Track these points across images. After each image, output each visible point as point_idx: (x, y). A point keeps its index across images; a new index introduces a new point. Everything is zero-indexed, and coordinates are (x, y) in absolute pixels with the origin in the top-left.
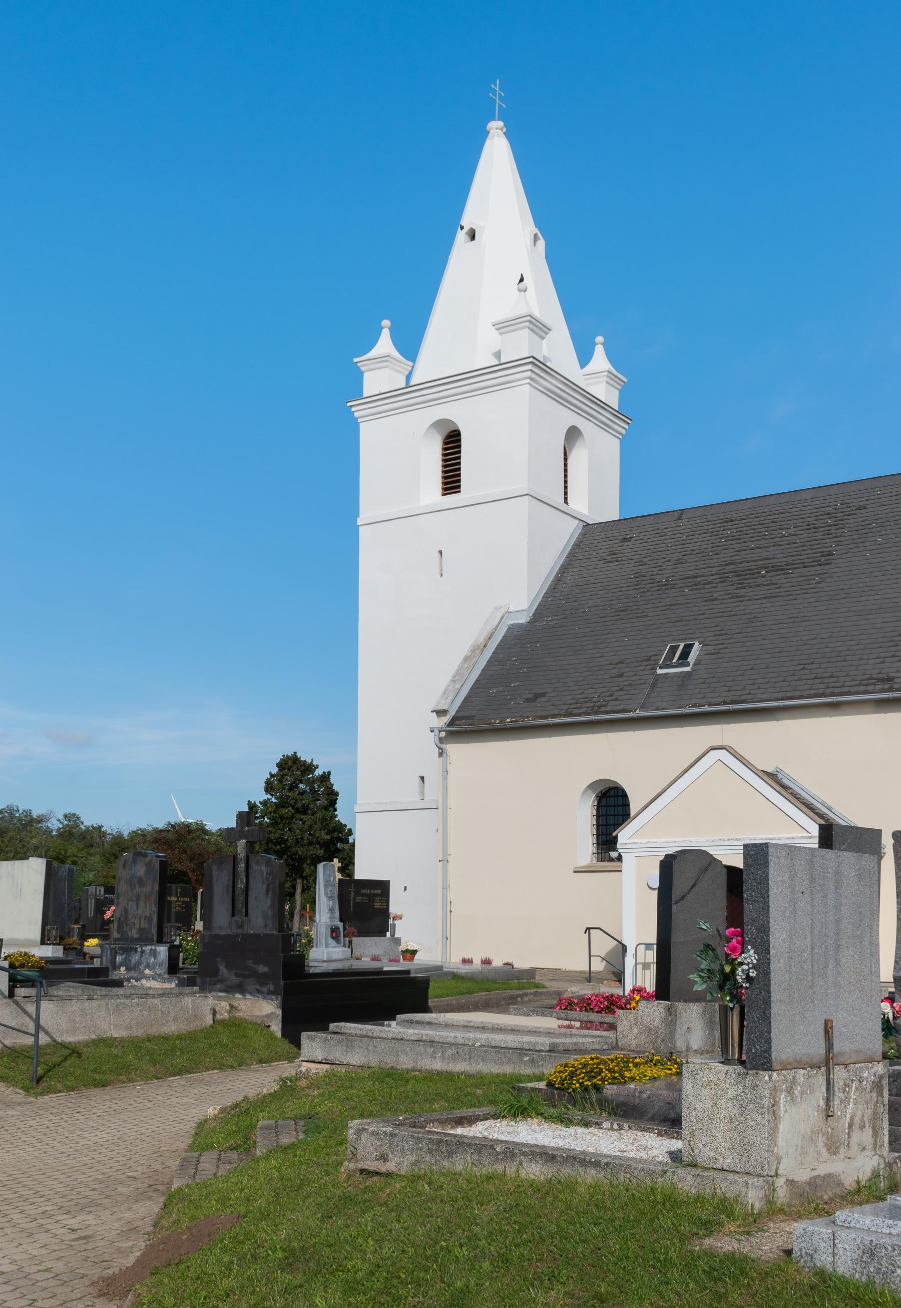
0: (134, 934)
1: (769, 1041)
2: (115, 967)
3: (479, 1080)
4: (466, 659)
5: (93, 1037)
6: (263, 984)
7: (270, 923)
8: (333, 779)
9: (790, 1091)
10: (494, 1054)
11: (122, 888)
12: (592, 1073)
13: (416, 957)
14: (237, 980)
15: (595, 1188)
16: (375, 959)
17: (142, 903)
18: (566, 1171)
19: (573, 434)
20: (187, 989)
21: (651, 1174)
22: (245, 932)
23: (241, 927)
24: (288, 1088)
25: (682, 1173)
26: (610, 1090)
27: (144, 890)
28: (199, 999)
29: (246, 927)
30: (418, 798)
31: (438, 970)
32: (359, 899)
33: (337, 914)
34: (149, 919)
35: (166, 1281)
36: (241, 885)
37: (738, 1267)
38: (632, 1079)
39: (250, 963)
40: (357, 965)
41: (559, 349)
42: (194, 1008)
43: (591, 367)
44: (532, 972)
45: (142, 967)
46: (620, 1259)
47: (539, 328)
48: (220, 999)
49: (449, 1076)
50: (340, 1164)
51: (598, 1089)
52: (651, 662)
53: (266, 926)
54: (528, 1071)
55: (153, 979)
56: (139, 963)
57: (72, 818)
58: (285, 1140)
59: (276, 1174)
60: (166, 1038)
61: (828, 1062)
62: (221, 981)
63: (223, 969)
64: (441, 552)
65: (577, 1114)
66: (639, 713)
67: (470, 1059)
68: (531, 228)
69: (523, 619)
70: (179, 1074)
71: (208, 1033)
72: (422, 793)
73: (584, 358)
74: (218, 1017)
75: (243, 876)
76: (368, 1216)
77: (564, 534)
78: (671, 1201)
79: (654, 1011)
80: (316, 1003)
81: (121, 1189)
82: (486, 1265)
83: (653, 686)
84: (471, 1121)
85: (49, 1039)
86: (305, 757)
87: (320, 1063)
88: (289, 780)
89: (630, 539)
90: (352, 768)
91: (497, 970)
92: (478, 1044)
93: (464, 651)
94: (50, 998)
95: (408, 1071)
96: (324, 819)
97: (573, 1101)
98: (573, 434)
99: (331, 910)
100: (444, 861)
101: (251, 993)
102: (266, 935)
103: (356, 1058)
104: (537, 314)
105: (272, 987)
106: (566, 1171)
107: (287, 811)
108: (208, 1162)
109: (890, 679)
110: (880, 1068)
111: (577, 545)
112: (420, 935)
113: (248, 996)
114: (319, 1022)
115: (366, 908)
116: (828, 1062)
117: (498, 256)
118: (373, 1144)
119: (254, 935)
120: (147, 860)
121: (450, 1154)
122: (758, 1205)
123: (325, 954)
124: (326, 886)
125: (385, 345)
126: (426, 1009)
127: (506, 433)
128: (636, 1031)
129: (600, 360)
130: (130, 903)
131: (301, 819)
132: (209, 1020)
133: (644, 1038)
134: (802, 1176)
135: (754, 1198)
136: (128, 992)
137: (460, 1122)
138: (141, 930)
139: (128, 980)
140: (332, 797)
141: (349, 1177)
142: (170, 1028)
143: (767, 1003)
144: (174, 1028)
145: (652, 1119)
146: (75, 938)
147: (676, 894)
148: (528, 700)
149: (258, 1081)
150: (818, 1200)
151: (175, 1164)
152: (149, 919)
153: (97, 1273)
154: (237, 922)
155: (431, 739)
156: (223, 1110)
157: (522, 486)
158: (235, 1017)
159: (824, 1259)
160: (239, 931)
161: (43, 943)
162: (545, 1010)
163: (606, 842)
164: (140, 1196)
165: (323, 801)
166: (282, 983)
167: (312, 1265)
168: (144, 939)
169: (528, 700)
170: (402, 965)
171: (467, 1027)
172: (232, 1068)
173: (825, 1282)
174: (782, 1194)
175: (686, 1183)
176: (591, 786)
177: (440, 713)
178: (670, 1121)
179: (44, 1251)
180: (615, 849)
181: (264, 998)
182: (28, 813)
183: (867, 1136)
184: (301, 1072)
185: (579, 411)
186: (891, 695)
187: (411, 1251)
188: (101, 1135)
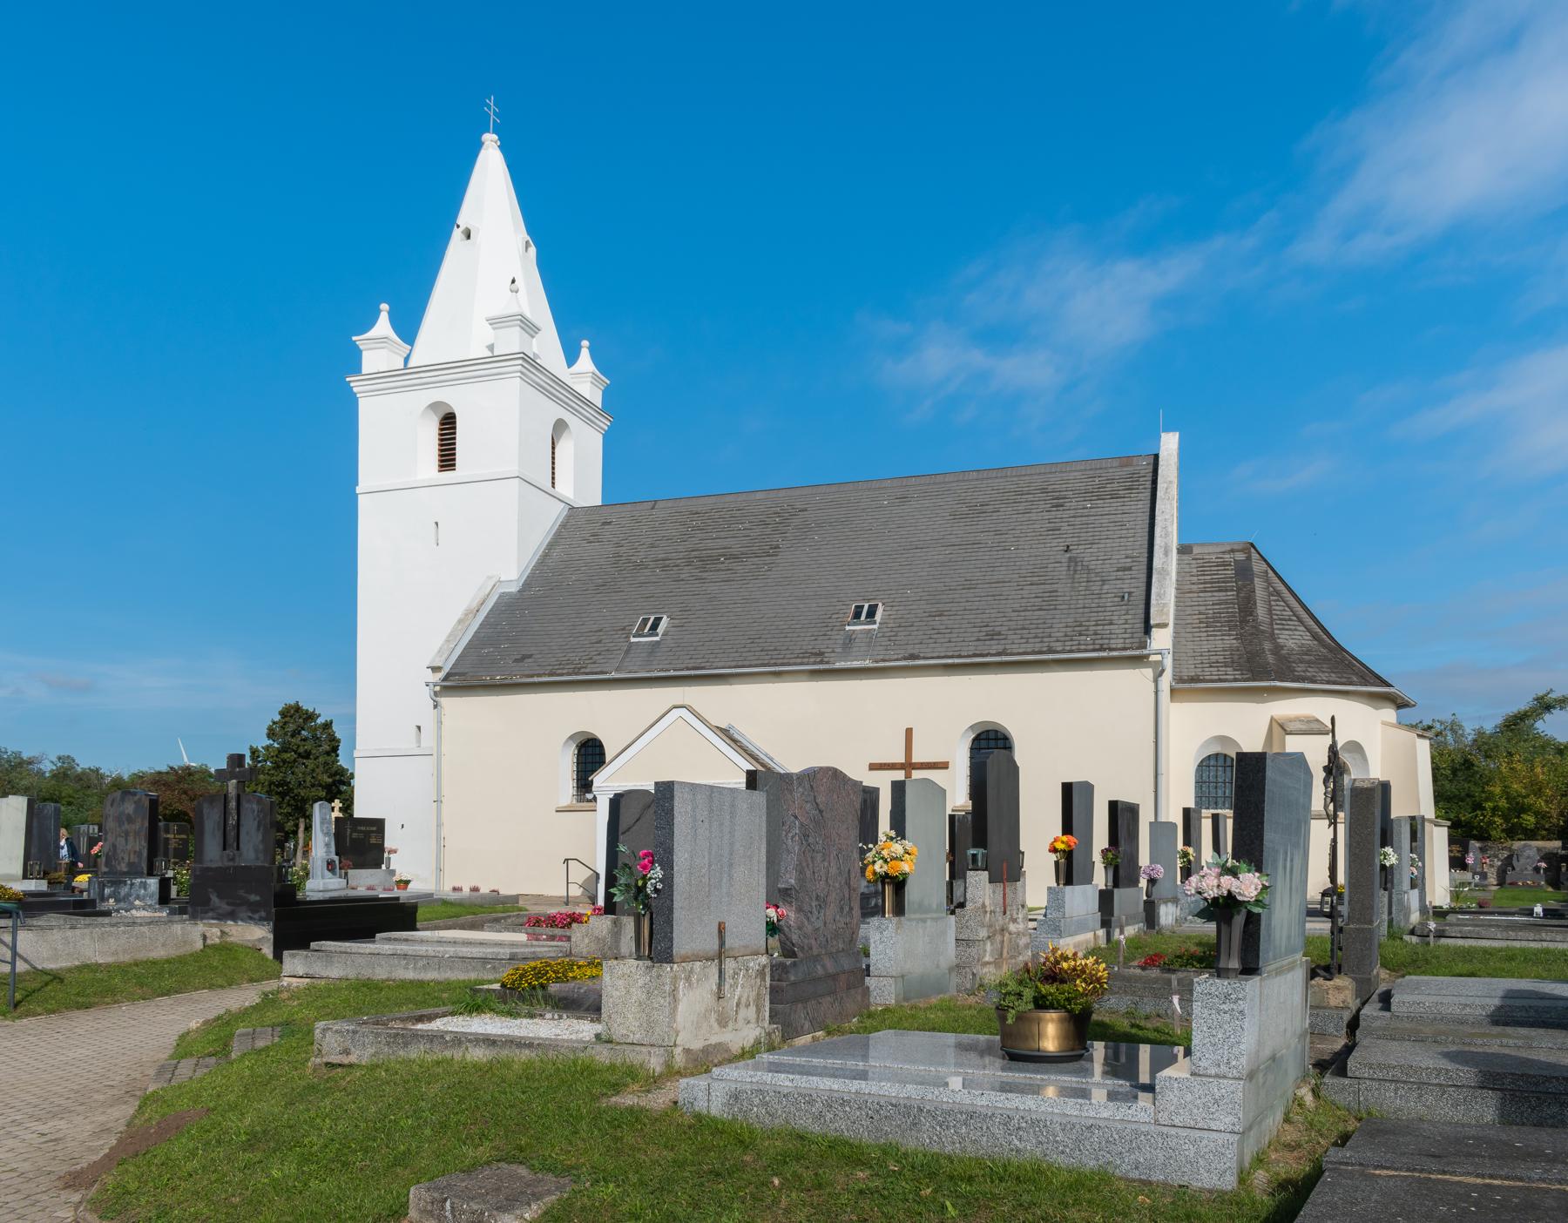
1: (671, 940)
2: (103, 899)
3: (447, 986)
4: (460, 621)
6: (254, 912)
7: (261, 856)
9: (688, 979)
11: (110, 824)
12: (539, 974)
14: (229, 908)
15: (528, 1065)
16: (370, 888)
17: (131, 839)
18: (505, 1053)
19: (560, 427)
20: (177, 917)
21: (574, 1050)
23: (233, 860)
24: (269, 1001)
25: (599, 1048)
26: (554, 988)
28: (189, 926)
30: (415, 745)
31: (428, 898)
32: (355, 835)
33: (333, 849)
34: (139, 854)
35: (131, 1169)
36: (232, 821)
37: (636, 1116)
38: (574, 978)
39: (241, 893)
40: (352, 893)
41: (548, 347)
43: (576, 368)
44: (516, 898)
46: (540, 1117)
47: (530, 328)
48: (211, 926)
49: (421, 984)
50: (307, 1060)
51: (543, 987)
52: (625, 631)
54: (491, 977)
57: (66, 760)
58: (260, 1044)
59: (247, 1072)
60: (154, 963)
61: (720, 955)
63: (214, 899)
65: (525, 1008)
66: (614, 675)
68: (523, 235)
69: (514, 589)
71: (196, 957)
72: (419, 741)
73: (571, 358)
74: (209, 942)
75: (234, 812)
76: (327, 1101)
77: (550, 516)
78: (589, 1070)
79: (603, 924)
80: (302, 924)
81: (96, 1096)
82: (428, 1132)
83: (627, 652)
84: (430, 1018)
85: (27, 967)
86: (307, 706)
88: (291, 727)
90: (352, 720)
91: (484, 896)
93: (459, 613)
94: (30, 928)
95: (383, 981)
96: (326, 763)
97: (522, 998)
98: (560, 427)
99: (327, 845)
100: (438, 801)
103: (335, 972)
104: (528, 315)
105: (263, 914)
106: (505, 1053)
108: (186, 1068)
109: (821, 654)
110: (764, 960)
111: (563, 526)
112: (412, 865)
114: (303, 944)
115: (362, 843)
116: (720, 955)
118: (334, 1040)
121: (406, 1045)
122: (658, 1069)
123: (321, 884)
124: (322, 823)
125: (383, 326)
126: (414, 929)
127: (497, 419)
129: (585, 362)
131: (304, 764)
132: (199, 945)
133: (593, 947)
134: (697, 1045)
135: (655, 1064)
136: (114, 921)
137: (420, 1019)
138: (130, 864)
139: (117, 911)
141: (315, 1070)
142: (159, 953)
143: (671, 910)
145: (587, 1010)
146: (62, 873)
147: (623, 826)
148: (516, 661)
149: (244, 997)
150: (702, 1062)
151: (152, 1072)
152: (139, 854)
153: (65, 1168)
155: (427, 692)
156: (206, 1022)
157: (514, 469)
159: (701, 1106)
161: (25, 877)
162: (515, 928)
163: (584, 785)
164: (117, 1101)
165: (326, 747)
167: (272, 1144)
168: (134, 872)
169: (516, 661)
170: (396, 893)
171: (440, 942)
172: (222, 987)
173: (702, 1122)
174: (679, 1060)
175: (603, 1055)
176: (571, 738)
177: (435, 669)
178: (588, 1006)
179: (10, 1154)
180: (590, 791)
182: (18, 755)
183: (751, 1012)
186: (821, 667)
187: (363, 1125)
188: (80, 1051)
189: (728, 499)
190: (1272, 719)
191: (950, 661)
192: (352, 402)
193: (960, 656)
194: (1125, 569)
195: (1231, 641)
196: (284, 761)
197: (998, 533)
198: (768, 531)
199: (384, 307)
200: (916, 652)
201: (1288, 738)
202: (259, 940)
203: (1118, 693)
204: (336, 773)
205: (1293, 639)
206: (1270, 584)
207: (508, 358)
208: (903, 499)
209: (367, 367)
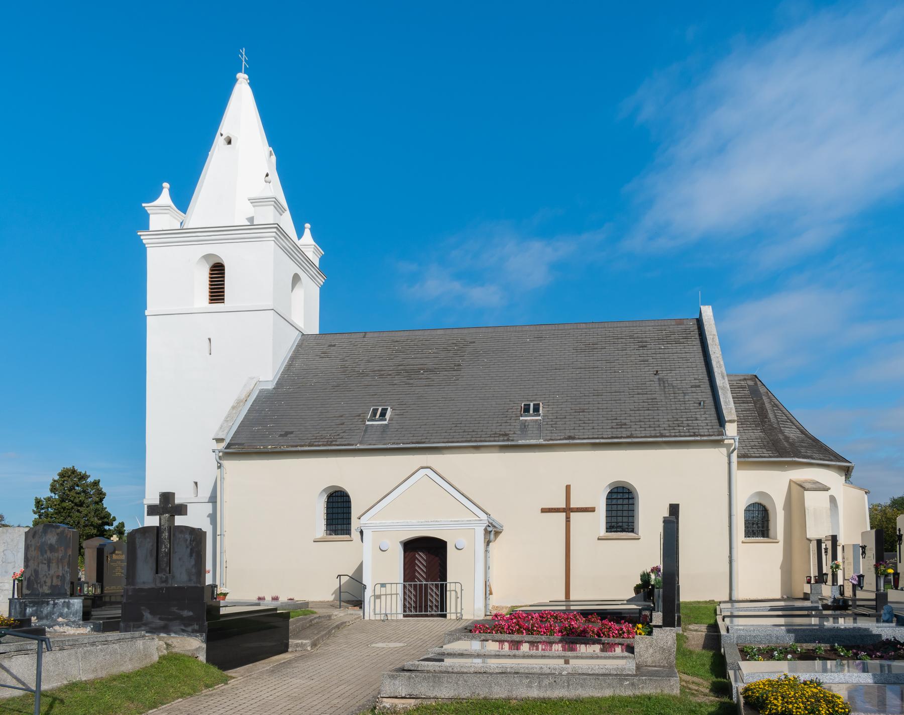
0: (46, 589)
4: (233, 408)
5: (65, 682)
8: (101, 485)
10: (593, 681)
13: (227, 597)
14: (162, 623)
17: (53, 565)
22: (169, 585)
23: (166, 581)
27: (56, 555)
29: (170, 581)
30: (193, 495)
39: (175, 609)
41: (287, 222)
42: (144, 648)
45: (54, 617)
53: (190, 580)
55: (67, 625)
56: (51, 613)
62: (145, 625)
63: (147, 616)
64: (210, 340)
66: (359, 446)
67: (568, 686)
69: (270, 386)
70: (155, 707)
73: (300, 234)
77: (291, 340)
83: (366, 431)
86: (80, 469)
87: (402, 698)
88: (68, 485)
89: (334, 345)
92: (565, 673)
93: (232, 403)
96: (97, 510)
101: (175, 633)
102: (189, 588)
105: (196, 627)
107: (67, 504)
109: (506, 435)
113: (173, 635)
117: (242, 161)
119: (178, 588)
120: (59, 531)
125: (165, 198)
128: (651, 651)
130: (40, 565)
133: (658, 656)
138: (52, 587)
140: (101, 495)
142: (128, 667)
144: (130, 666)
148: (281, 435)
154: (161, 578)
157: (269, 304)
158: (172, 653)
160: (164, 585)
166: (206, 623)
168: (57, 593)
169: (281, 435)
176: (325, 490)
177: (219, 440)
181: (189, 635)
184: (384, 707)
185: (300, 265)
186: (510, 443)
189: (417, 333)
190: (790, 481)
191: (597, 441)
192: (140, 252)
193: (603, 438)
194: (696, 387)
195: (758, 433)
196: (64, 508)
197: (607, 361)
198: (451, 354)
199: (166, 185)
200: (572, 435)
201: (807, 494)
202: (197, 649)
203: (711, 460)
204: (104, 517)
205: (792, 433)
206: (771, 400)
207: (266, 226)
208: (540, 338)
209: (152, 227)
